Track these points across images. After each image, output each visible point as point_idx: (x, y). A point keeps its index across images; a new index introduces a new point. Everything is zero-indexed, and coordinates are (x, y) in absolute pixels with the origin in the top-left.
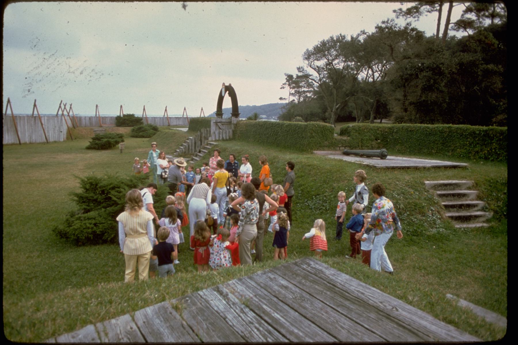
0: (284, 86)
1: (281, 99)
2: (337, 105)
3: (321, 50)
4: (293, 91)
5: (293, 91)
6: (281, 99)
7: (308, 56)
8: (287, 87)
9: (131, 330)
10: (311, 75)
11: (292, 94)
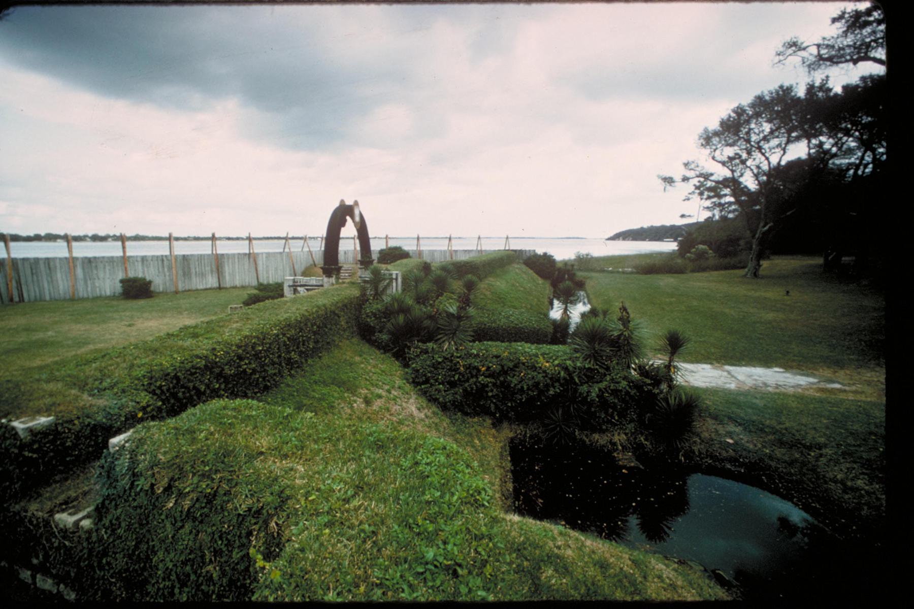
0: (690, 196)
1: (683, 216)
2: (764, 226)
3: (733, 127)
4: (708, 203)
5: (708, 203)
6: (683, 216)
7: (707, 139)
8: (696, 198)
9: (119, 592)
10: (712, 175)
11: (708, 208)
